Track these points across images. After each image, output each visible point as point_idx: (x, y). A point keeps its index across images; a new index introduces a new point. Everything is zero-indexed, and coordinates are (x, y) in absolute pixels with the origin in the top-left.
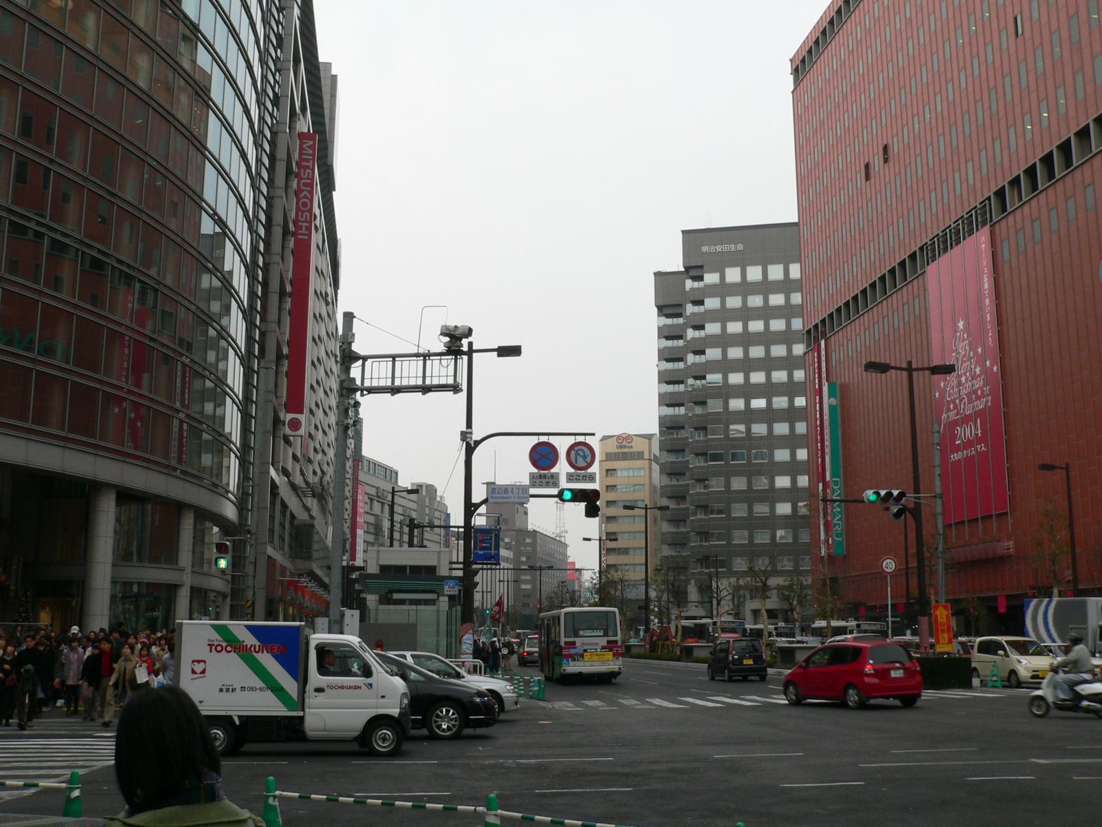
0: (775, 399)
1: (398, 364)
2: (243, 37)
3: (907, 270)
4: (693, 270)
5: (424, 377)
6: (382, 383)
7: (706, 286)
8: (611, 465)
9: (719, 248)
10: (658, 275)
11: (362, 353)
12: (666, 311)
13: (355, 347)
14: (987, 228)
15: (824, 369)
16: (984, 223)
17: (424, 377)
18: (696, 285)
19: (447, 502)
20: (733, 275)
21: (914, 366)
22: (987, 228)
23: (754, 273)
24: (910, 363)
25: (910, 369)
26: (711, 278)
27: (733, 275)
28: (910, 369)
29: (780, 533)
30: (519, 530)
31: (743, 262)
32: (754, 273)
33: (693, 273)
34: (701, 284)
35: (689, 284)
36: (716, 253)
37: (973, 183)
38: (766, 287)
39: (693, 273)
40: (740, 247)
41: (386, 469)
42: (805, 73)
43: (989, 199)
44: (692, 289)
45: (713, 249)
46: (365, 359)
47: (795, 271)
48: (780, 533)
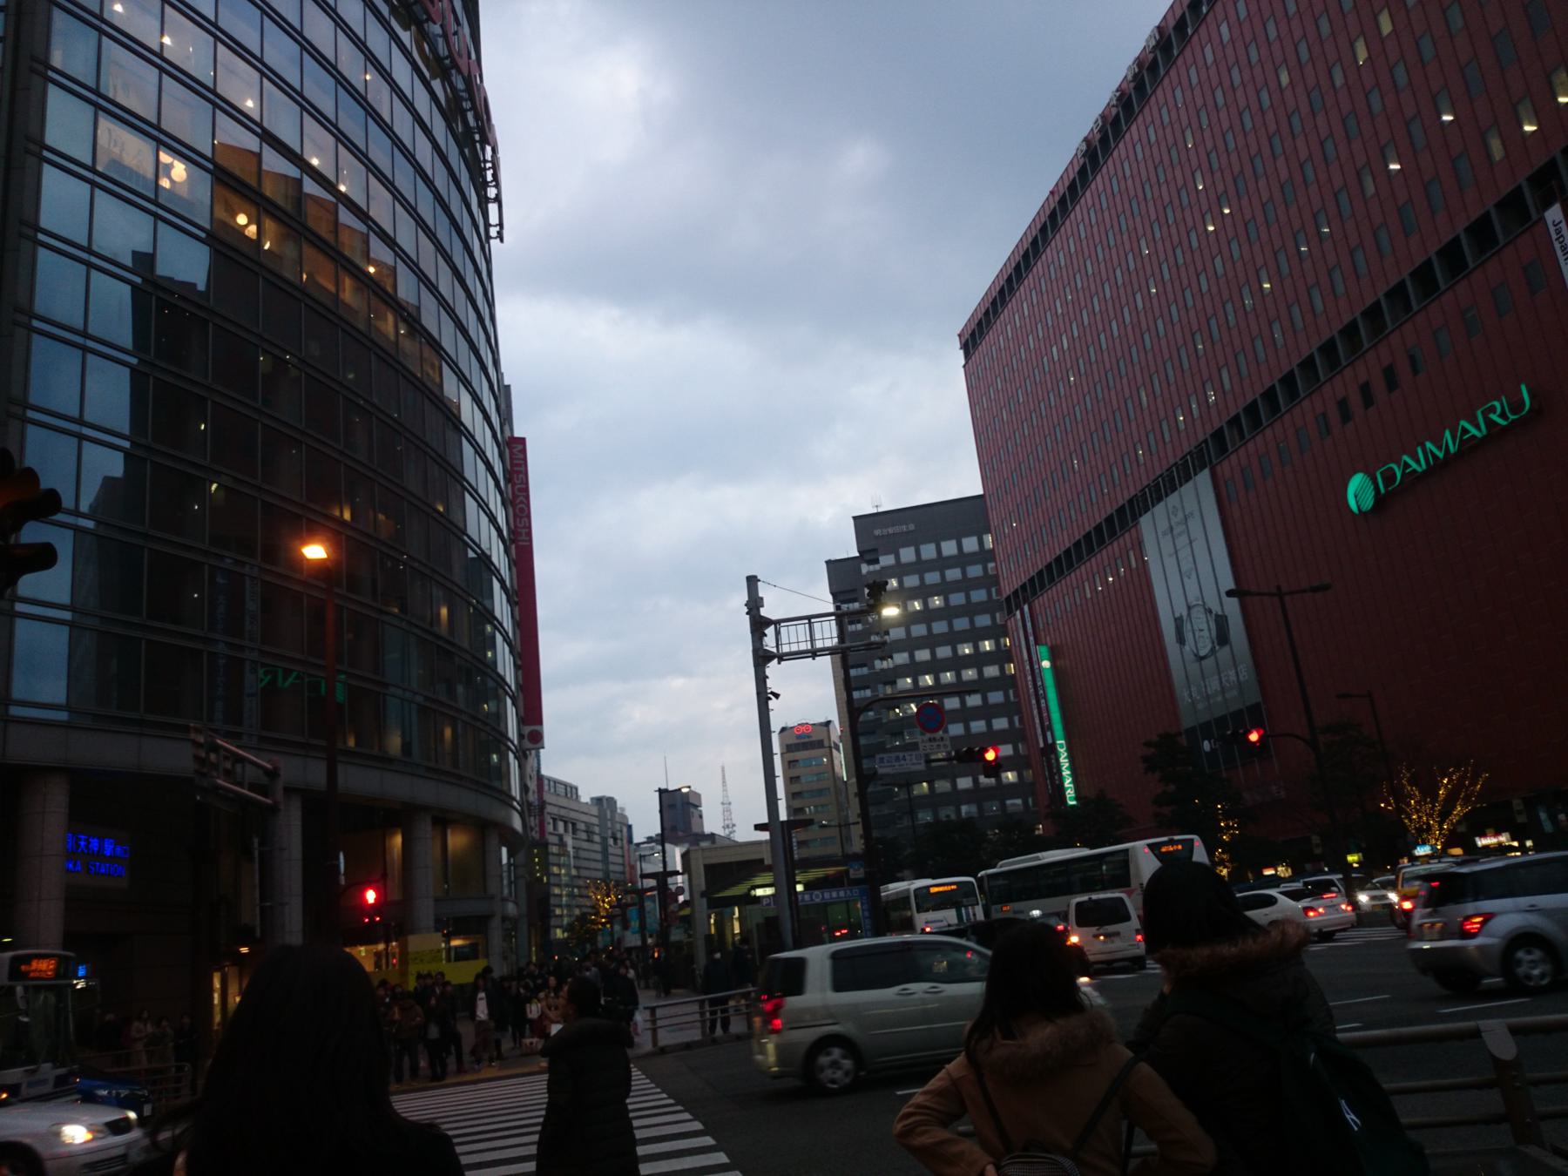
0: (942, 675)
1: (817, 626)
2: (472, 333)
3: (1122, 520)
4: (868, 553)
5: (812, 640)
6: (803, 647)
7: (883, 568)
8: (791, 756)
9: (891, 530)
10: (828, 563)
11: (774, 617)
12: (841, 597)
13: (764, 612)
14: (1206, 473)
15: (1030, 630)
16: (1202, 468)
17: (812, 640)
18: (872, 568)
19: (627, 813)
20: (907, 555)
21: (1284, 589)
22: (1206, 473)
23: (928, 551)
24: (1279, 588)
25: (1280, 594)
26: (887, 560)
27: (907, 555)
28: (1280, 594)
29: (964, 809)
30: (696, 835)
31: (915, 541)
32: (928, 551)
33: (868, 557)
34: (877, 567)
35: (865, 568)
36: (889, 535)
37: (1187, 423)
38: (942, 563)
39: (868, 557)
40: (912, 527)
41: (566, 785)
42: (975, 346)
43: (1206, 441)
44: (869, 573)
45: (885, 532)
46: (777, 623)
47: (989, 540)
48: (964, 809)
